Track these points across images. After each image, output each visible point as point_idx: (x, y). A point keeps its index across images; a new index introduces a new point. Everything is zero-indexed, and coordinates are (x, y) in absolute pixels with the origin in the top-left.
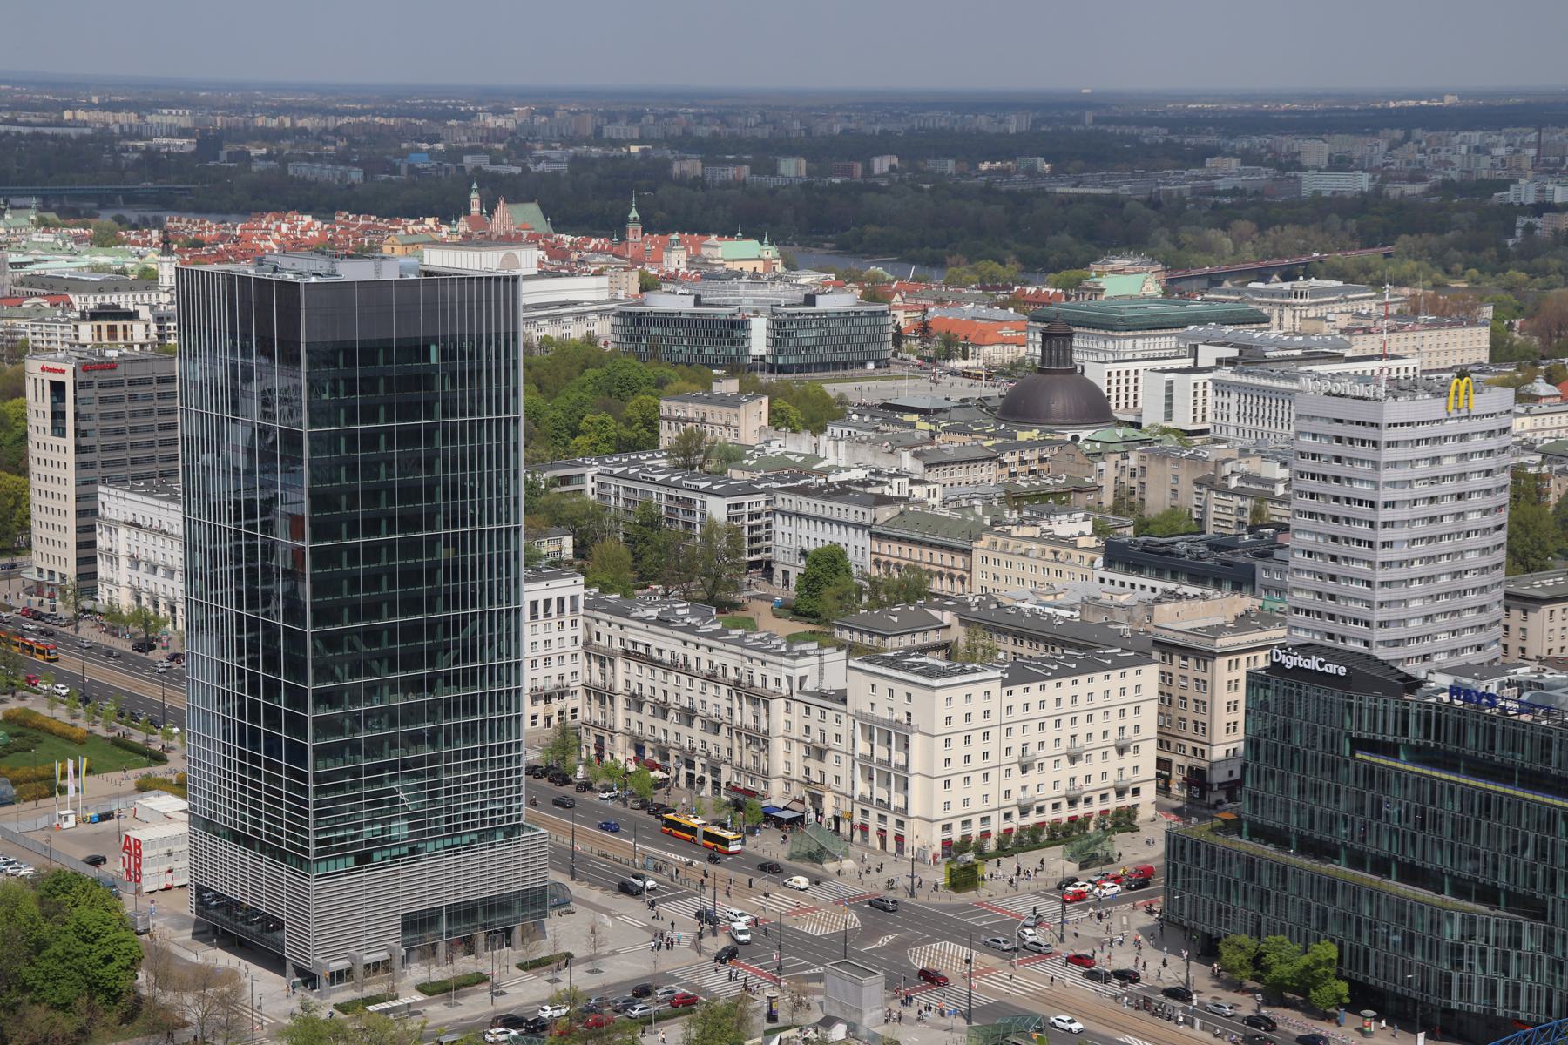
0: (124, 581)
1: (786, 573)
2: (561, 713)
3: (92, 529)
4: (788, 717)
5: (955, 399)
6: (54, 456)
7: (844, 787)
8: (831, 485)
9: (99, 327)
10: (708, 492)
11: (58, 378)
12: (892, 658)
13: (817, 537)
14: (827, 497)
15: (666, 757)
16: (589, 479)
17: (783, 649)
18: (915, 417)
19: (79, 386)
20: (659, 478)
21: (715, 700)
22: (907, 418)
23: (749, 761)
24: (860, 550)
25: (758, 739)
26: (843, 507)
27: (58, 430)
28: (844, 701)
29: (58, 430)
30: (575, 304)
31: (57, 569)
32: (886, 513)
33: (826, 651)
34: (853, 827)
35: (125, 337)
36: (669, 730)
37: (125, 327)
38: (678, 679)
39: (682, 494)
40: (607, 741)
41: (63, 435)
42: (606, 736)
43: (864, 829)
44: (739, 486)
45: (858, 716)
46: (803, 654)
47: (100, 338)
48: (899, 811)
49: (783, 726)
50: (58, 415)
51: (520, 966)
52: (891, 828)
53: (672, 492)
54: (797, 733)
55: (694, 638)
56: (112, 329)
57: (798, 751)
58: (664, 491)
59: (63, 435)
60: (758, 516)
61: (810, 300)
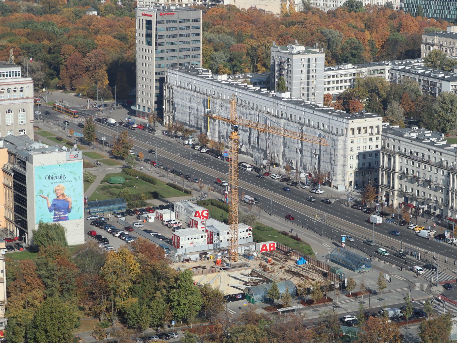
10: (443, 79)
11: (149, 18)
16: (387, 71)
19: (158, 22)
20: (420, 72)
27: (149, 43)
29: (149, 43)
39: (430, 80)
50: (149, 36)
53: (426, 79)
55: (433, 148)
59: (151, 45)
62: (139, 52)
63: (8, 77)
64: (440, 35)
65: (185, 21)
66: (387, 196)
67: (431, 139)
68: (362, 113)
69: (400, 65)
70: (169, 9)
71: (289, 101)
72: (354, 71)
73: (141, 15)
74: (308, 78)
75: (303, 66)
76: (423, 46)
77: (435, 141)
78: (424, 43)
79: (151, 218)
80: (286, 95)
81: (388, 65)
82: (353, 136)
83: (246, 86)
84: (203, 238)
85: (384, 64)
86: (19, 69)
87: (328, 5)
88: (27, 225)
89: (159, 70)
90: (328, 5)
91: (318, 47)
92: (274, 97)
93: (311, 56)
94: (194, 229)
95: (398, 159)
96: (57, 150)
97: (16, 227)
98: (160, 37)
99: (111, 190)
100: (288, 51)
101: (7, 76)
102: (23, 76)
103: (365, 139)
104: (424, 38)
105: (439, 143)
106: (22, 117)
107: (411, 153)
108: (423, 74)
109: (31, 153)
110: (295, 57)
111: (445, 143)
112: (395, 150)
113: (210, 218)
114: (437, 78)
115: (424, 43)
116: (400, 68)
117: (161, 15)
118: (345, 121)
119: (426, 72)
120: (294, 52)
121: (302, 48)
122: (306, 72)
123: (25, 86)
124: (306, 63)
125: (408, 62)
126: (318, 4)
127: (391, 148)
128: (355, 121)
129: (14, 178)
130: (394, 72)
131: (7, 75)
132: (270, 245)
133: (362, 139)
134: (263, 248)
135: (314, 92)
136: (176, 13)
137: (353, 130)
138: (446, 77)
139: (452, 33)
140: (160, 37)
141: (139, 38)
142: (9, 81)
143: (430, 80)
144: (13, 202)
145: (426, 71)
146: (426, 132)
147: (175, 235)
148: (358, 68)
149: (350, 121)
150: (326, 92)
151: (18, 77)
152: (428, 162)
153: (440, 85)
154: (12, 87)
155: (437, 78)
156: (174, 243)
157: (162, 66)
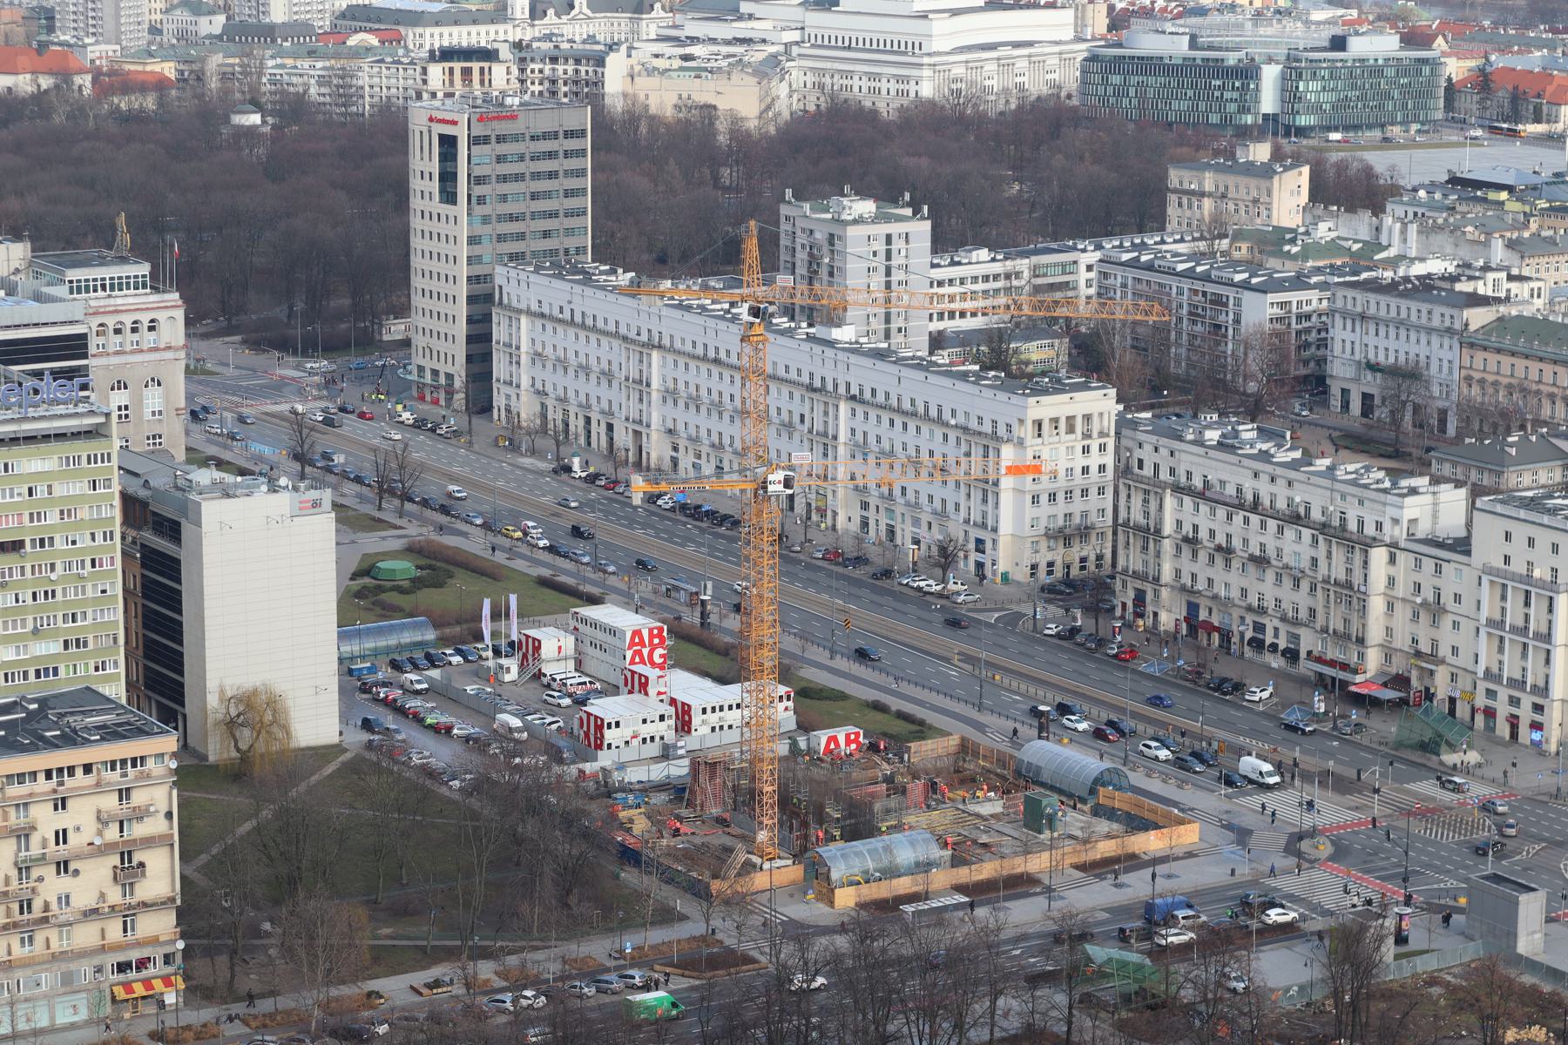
0: (525, 382)
1: (1345, 392)
2: (1083, 560)
3: (487, 318)
4: (1392, 571)
5: (1546, 174)
6: (442, 227)
7: (1464, 660)
8: (1407, 279)
9: (451, 70)
10: (1245, 286)
11: (448, 130)
12: (1532, 499)
13: (1390, 348)
14: (1405, 295)
15: (428, 657)
16: (1083, 268)
17: (1387, 484)
18: (1504, 195)
19: (474, 141)
20: (1180, 267)
21: (1296, 547)
22: (1492, 195)
23: (1336, 624)
24: (1443, 363)
25: (1351, 593)
26: (1425, 307)
27: (449, 197)
28: (1468, 553)
29: (449, 197)
30: (1030, 44)
31: (443, 368)
32: (1478, 318)
33: (1443, 487)
34: (1473, 711)
35: (482, 82)
36: (1230, 581)
37: (482, 70)
38: (1246, 521)
39: (1211, 288)
40: (1149, 596)
41: (454, 202)
42: (1149, 589)
43: (1490, 713)
44: (1285, 280)
45: (1488, 570)
46: (1413, 491)
47: (452, 82)
48: (1535, 689)
49: (1383, 582)
50: (448, 178)
51: (1076, 867)
52: (1525, 713)
53: (1198, 285)
54: (1401, 590)
55: (1269, 468)
56: (467, 72)
57: (1402, 613)
58: (1186, 285)
59: (454, 202)
60: (1308, 317)
61: (1339, 43)
62: (416, 223)
63: (117, 293)
64: (1219, 169)
65: (546, 136)
66: (1140, 599)
67: (1259, 446)
68: (1059, 381)
69: (1119, 247)
70: (502, 105)
71: (855, 349)
72: (997, 268)
73: (425, 120)
74: (888, 285)
75: (875, 254)
76: (1173, 198)
77: (1272, 451)
78: (1175, 191)
79: (508, 670)
80: (844, 334)
81: (1084, 251)
82: (1039, 440)
83: (728, 312)
84: (668, 722)
85: (1074, 248)
86: (144, 269)
87: (884, 92)
88: (182, 695)
89: (478, 270)
90: (884, 92)
91: (909, 205)
92: (811, 338)
93: (895, 228)
94: (636, 696)
95: (1169, 501)
96: (264, 488)
97: (150, 698)
98: (480, 180)
99: (385, 597)
100: (829, 216)
101: (112, 289)
102: (155, 289)
103: (1071, 449)
104: (1175, 177)
105: (1284, 456)
106: (153, 399)
107: (1206, 482)
108: (1189, 274)
109: (193, 496)
110: (851, 231)
111: (1297, 454)
112: (1162, 477)
113: (672, 666)
114: (1232, 284)
115: (1175, 191)
116: (1125, 257)
117: (481, 119)
118: (1015, 399)
119: (1199, 269)
120: (850, 218)
121: (867, 207)
122: (882, 270)
123: (161, 316)
124: (880, 247)
125: (1137, 241)
126: (856, 89)
127: (1148, 471)
128: (1044, 399)
129: (143, 565)
130: (1107, 268)
131: (112, 286)
132: (847, 736)
133: (1063, 449)
134: (828, 744)
135: (903, 325)
136: (522, 116)
137: (1039, 424)
138: (1254, 281)
139: (1252, 163)
140: (480, 180)
141: (416, 184)
142: (119, 301)
143: (1211, 288)
144: (141, 631)
145: (1198, 264)
146: (1241, 428)
147: (589, 714)
148: (1006, 259)
149: (1032, 400)
150: (936, 326)
151: (141, 291)
152: (1255, 507)
153: (1238, 302)
154: (128, 320)
155: (1232, 284)
156: (594, 735)
157: (485, 260)
